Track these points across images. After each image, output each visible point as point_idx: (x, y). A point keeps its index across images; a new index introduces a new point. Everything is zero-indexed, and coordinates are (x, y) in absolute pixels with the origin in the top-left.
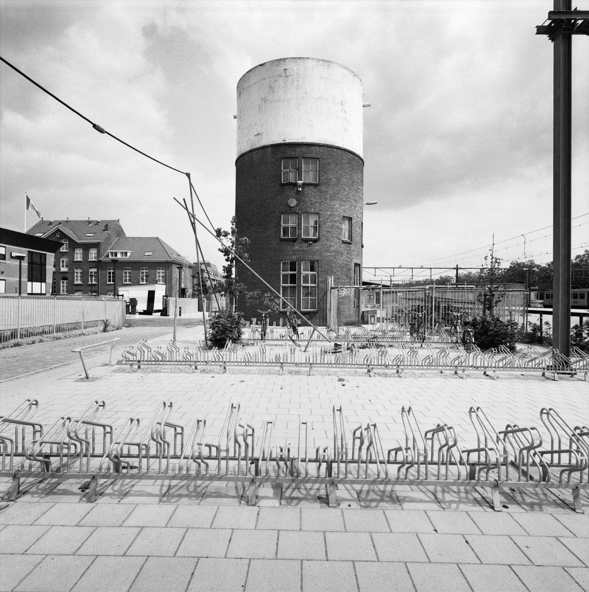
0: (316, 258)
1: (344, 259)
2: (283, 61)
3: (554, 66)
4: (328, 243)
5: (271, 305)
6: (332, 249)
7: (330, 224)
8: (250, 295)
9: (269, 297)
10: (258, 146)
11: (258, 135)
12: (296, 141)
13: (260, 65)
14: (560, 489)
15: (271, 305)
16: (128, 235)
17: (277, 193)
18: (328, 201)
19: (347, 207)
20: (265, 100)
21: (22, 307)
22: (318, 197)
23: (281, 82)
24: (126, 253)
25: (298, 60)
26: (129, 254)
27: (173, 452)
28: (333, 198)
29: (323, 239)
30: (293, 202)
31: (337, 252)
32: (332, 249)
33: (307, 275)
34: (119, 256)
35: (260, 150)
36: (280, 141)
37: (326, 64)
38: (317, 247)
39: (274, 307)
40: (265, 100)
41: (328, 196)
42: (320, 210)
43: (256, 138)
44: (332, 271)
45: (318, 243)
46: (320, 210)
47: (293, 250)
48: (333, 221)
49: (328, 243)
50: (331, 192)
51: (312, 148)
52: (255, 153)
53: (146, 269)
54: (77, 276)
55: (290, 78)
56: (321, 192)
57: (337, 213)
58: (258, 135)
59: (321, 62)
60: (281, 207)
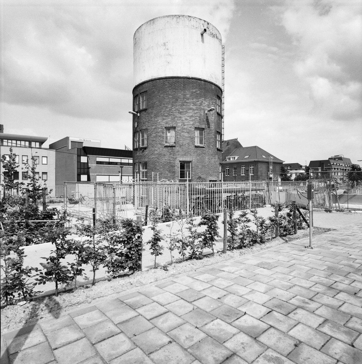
0: (146, 160)
1: (166, 158)
4: (153, 149)
6: (156, 152)
7: (154, 135)
14: (22, 349)
16: (244, 146)
18: (153, 119)
19: (169, 120)
22: (147, 118)
24: (235, 158)
26: (236, 158)
28: (156, 116)
29: (150, 146)
31: (160, 154)
32: (156, 152)
33: (143, 172)
34: (231, 159)
37: (152, 22)
38: (146, 153)
41: (153, 116)
42: (148, 126)
44: (156, 168)
45: (147, 150)
46: (148, 126)
48: (157, 132)
49: (153, 149)
50: (155, 112)
51: (144, 86)
53: (244, 167)
54: (251, 171)
56: (149, 114)
57: (159, 126)
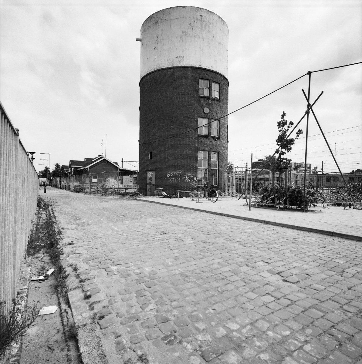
2: (199, 10)
3: (140, 121)
5: (191, 182)
8: (171, 175)
9: (189, 176)
10: (179, 65)
11: (179, 57)
12: (208, 68)
13: (181, 7)
15: (191, 182)
17: (196, 102)
20: (185, 33)
21: (7, 143)
23: (198, 24)
25: (209, 12)
27: (353, 242)
30: (207, 110)
35: (182, 69)
36: (198, 66)
39: (193, 183)
40: (185, 33)
43: (177, 59)
47: (206, 144)
52: (176, 70)
55: (204, 23)
58: (179, 57)
59: (221, 19)
60: (199, 113)
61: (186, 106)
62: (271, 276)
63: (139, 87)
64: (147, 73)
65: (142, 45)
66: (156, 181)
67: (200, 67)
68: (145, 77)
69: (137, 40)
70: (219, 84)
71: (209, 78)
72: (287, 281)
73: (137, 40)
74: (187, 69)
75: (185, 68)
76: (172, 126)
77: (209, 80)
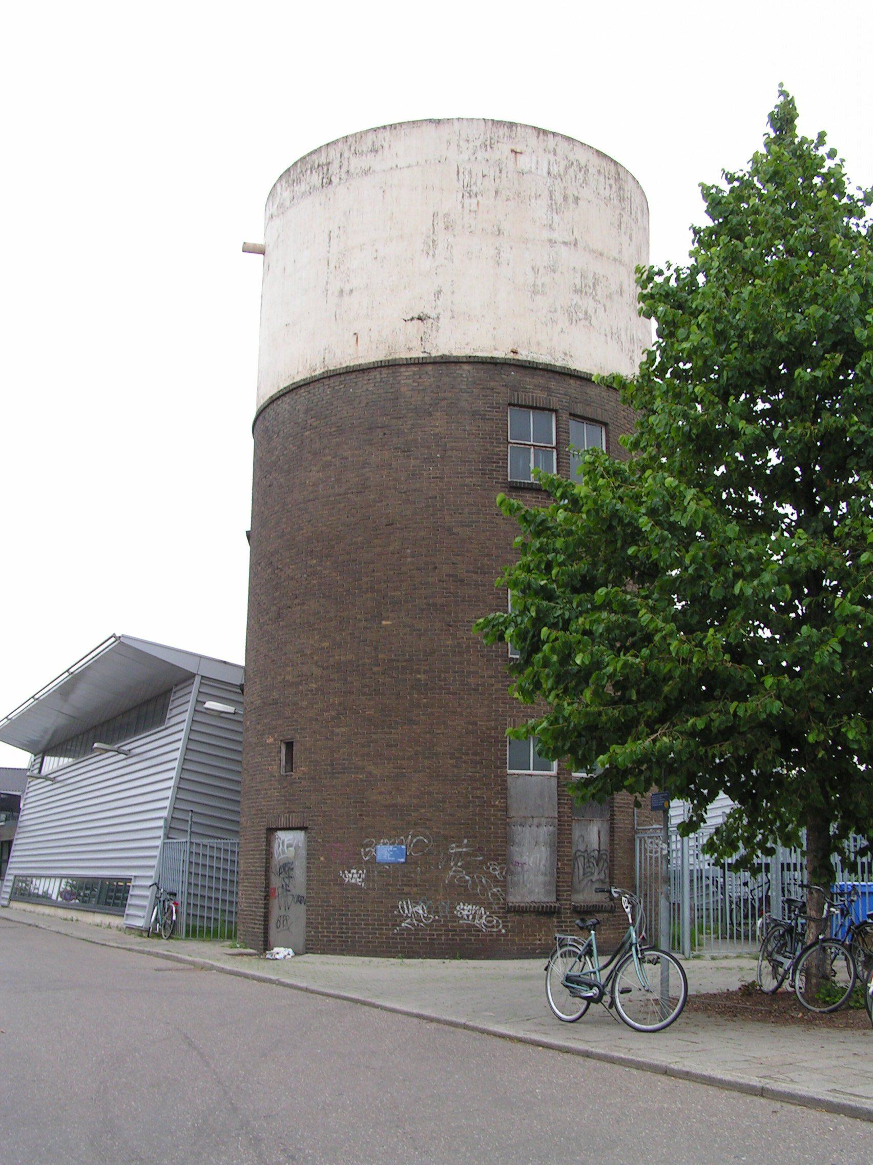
3: (248, 618)
36: (501, 353)
52: (406, 372)
61: (449, 529)
62: (515, 352)
63: (249, 547)
64: (284, 384)
65: (267, 268)
66: (309, 880)
67: (511, 356)
68: (273, 400)
69: (248, 249)
70: (606, 425)
71: (554, 403)
72: (783, 870)
73: (248, 249)
74: (453, 367)
75: (446, 362)
76: (387, 619)
77: (556, 411)
